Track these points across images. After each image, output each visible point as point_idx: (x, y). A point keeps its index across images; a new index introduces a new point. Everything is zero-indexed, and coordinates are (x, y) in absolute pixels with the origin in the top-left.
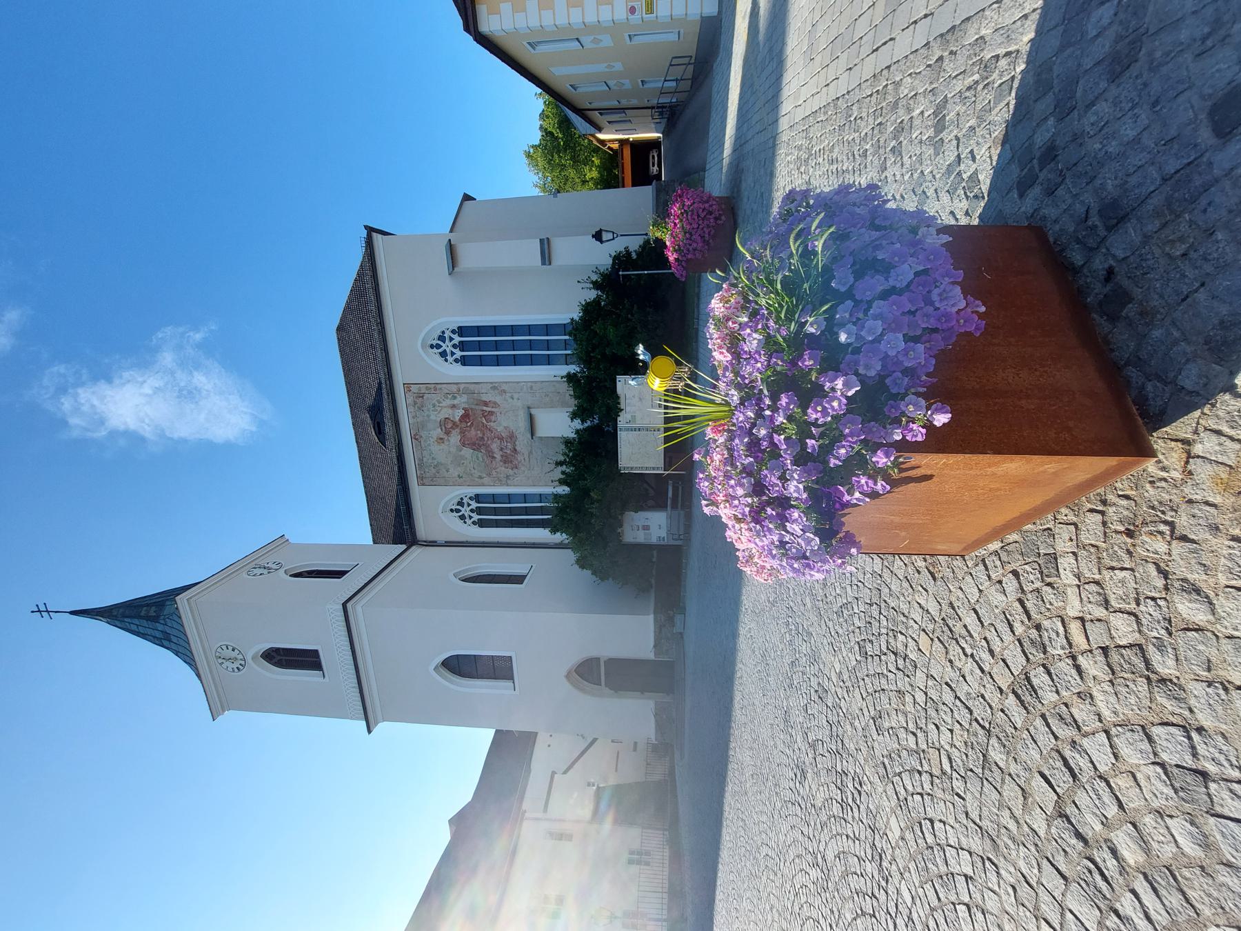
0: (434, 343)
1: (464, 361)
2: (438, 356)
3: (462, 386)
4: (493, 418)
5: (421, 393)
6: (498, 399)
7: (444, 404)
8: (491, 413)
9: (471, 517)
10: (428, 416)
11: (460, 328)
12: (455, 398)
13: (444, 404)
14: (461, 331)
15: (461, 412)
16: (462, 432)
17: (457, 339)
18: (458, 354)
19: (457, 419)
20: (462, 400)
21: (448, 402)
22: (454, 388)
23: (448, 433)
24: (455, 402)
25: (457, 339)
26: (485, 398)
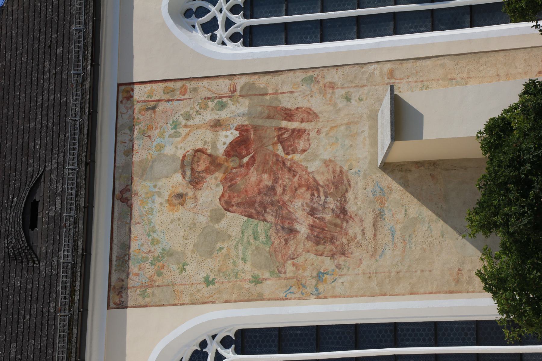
1: (250, 37)
3: (242, 81)
4: (301, 144)
5: (177, 86)
6: (316, 103)
8: (298, 133)
9: (229, 23)
10: (160, 147)
11: (242, 333)
12: (222, 106)
13: (197, 120)
15: (229, 136)
16: (229, 182)
19: (221, 149)
20: (238, 111)
21: (209, 116)
22: (224, 86)
23: (196, 182)
24: (223, 115)
26: (287, 102)
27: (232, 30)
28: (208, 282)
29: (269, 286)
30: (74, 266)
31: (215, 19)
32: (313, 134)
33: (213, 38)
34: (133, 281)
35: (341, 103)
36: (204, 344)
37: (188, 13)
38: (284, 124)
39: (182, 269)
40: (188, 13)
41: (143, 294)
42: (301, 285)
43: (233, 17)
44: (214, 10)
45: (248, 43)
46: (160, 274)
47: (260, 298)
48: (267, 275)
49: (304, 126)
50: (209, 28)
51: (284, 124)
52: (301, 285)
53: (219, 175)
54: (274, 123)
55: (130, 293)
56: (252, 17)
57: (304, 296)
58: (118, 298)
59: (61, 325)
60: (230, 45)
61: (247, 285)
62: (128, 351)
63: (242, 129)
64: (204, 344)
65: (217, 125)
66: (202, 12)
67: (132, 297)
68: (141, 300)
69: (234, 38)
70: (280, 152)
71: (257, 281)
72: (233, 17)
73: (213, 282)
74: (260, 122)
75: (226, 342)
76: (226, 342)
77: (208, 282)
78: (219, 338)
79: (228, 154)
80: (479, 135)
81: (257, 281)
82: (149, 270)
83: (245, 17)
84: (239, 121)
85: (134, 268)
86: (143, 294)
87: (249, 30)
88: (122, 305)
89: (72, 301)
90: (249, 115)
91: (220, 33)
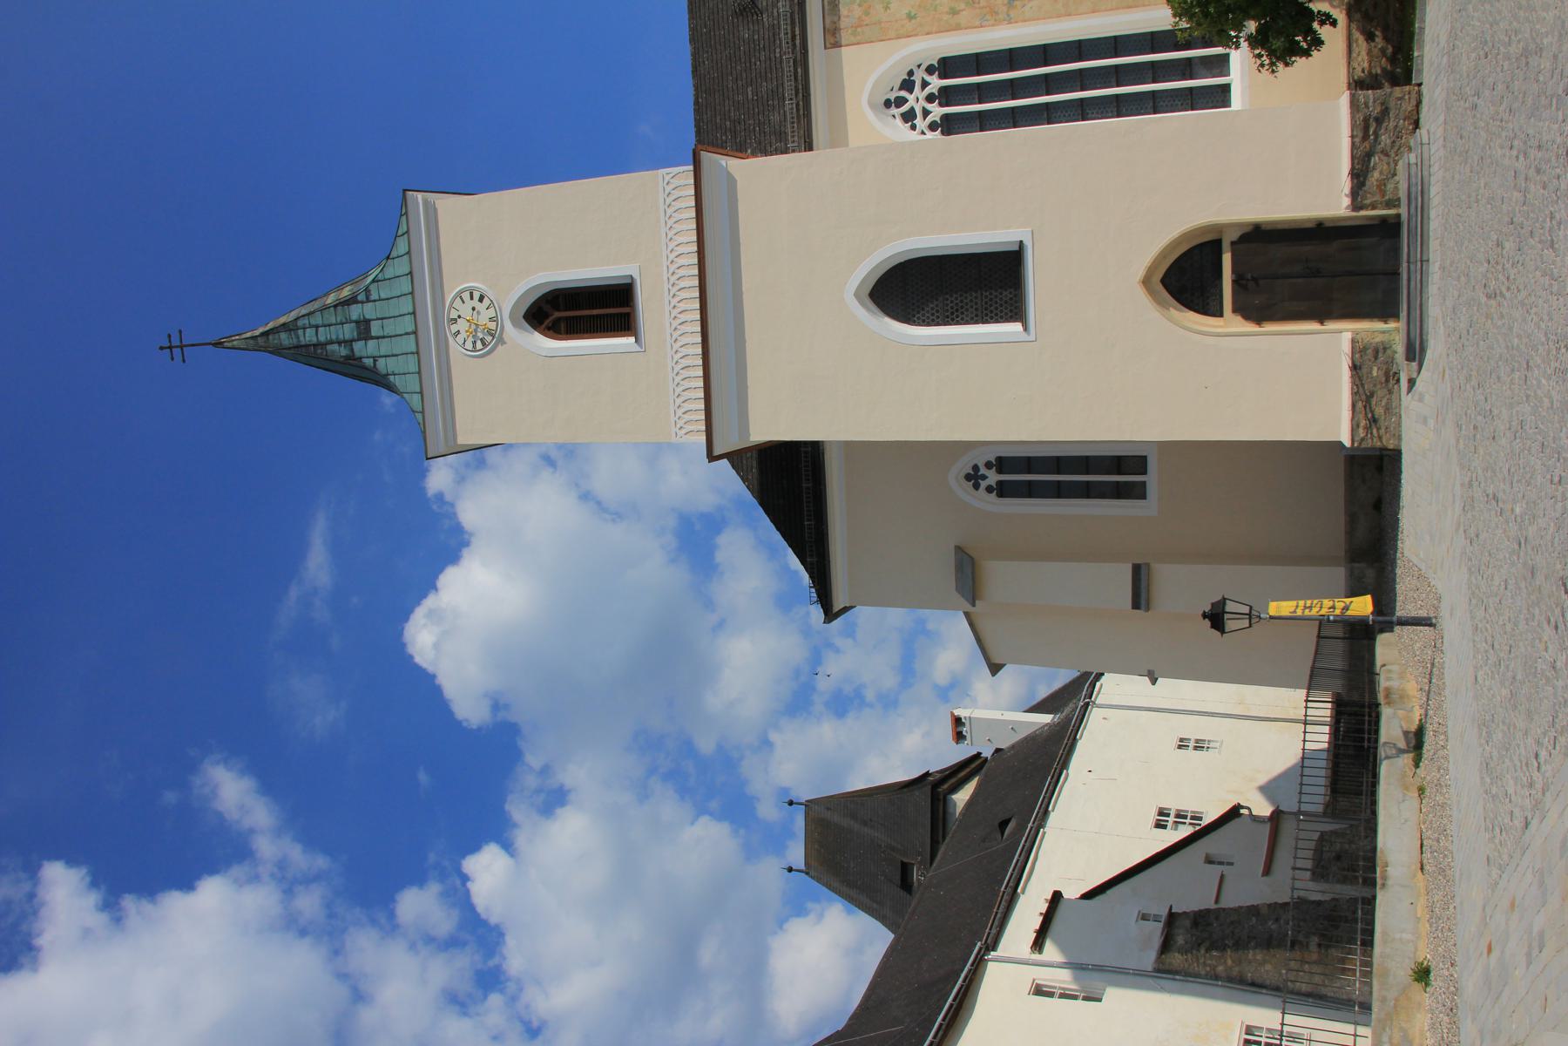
0: (892, 97)
2: (899, 121)
9: (926, 113)
14: (946, 66)
17: (936, 83)
18: (937, 112)
25: (936, 83)
27: (930, 119)
28: (910, 17)
29: (964, 17)
30: (792, 14)
31: (912, 109)
33: (913, 128)
34: (844, 23)
36: (911, 73)
37: (888, 104)
39: (887, 8)
40: (888, 104)
41: (854, 34)
42: (994, 13)
43: (929, 107)
44: (911, 98)
45: (1001, 495)
46: (867, 13)
47: (958, 27)
48: (962, 6)
50: (909, 117)
52: (994, 13)
55: (843, 33)
56: (947, 105)
57: (997, 23)
58: (833, 38)
59: (788, 68)
60: (930, 135)
61: (945, 17)
62: (847, 83)
64: (911, 73)
66: (900, 102)
67: (845, 36)
68: (853, 40)
69: (933, 127)
71: (954, 12)
72: (929, 107)
73: (914, 17)
75: (930, 70)
76: (930, 70)
77: (910, 17)
78: (924, 67)
80: (1229, 942)
81: (954, 12)
82: (858, 12)
83: (941, 105)
85: (843, 11)
86: (854, 34)
87: (945, 117)
88: (837, 45)
89: (794, 45)
91: (918, 121)
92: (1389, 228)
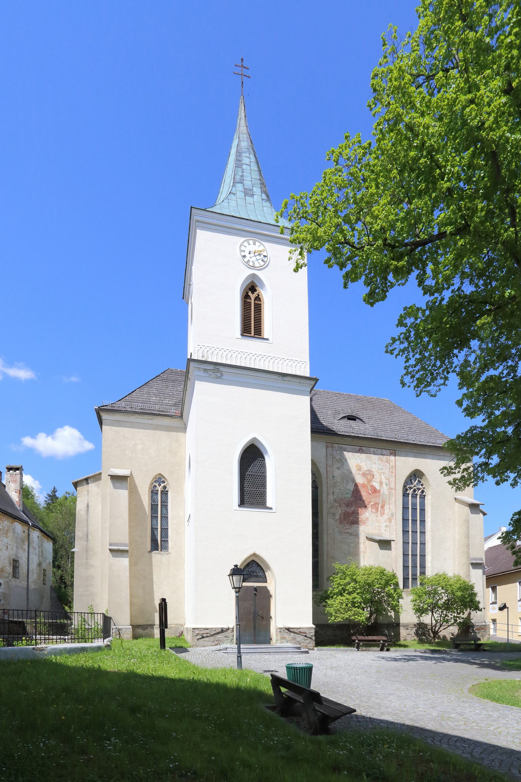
4: (374, 511)
7: (383, 477)
8: (377, 510)
10: (375, 463)
12: (387, 485)
15: (378, 488)
19: (374, 484)
21: (384, 480)
24: (384, 485)
26: (387, 507)
32: (377, 514)
35: (385, 524)
38: (380, 505)
49: (379, 512)
51: (380, 505)
53: (366, 483)
54: (380, 502)
63: (379, 491)
65: (381, 483)
70: (372, 503)
74: (381, 497)
79: (372, 486)
84: (382, 490)
90: (384, 493)
92: (268, 640)
